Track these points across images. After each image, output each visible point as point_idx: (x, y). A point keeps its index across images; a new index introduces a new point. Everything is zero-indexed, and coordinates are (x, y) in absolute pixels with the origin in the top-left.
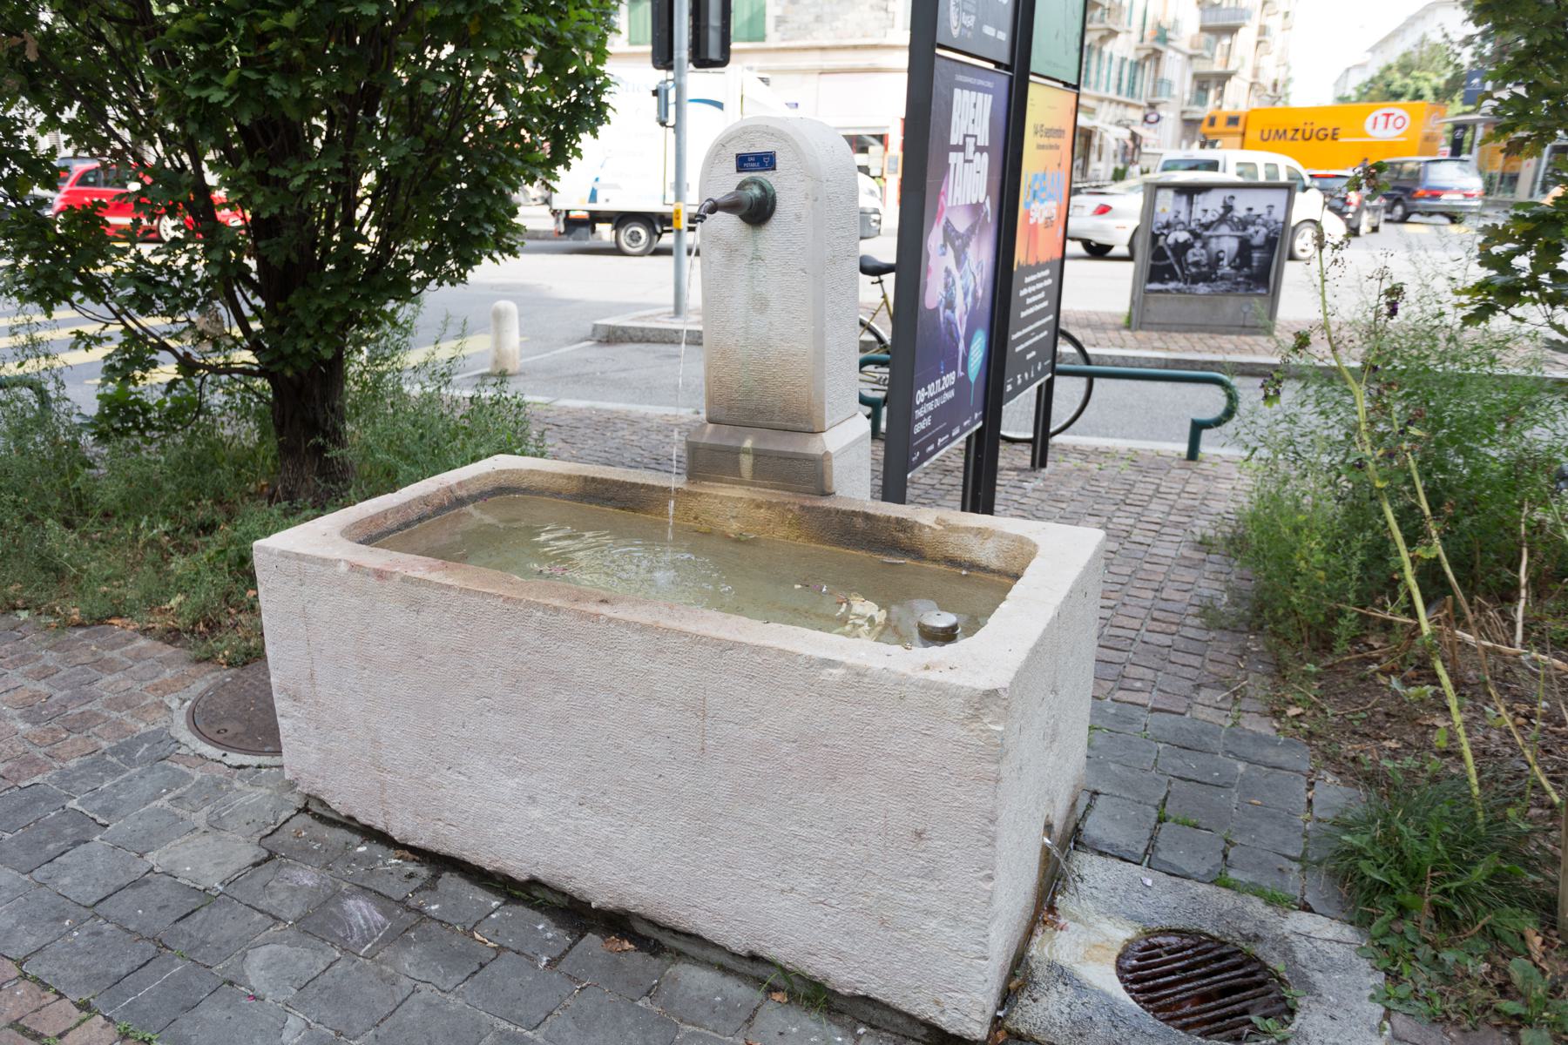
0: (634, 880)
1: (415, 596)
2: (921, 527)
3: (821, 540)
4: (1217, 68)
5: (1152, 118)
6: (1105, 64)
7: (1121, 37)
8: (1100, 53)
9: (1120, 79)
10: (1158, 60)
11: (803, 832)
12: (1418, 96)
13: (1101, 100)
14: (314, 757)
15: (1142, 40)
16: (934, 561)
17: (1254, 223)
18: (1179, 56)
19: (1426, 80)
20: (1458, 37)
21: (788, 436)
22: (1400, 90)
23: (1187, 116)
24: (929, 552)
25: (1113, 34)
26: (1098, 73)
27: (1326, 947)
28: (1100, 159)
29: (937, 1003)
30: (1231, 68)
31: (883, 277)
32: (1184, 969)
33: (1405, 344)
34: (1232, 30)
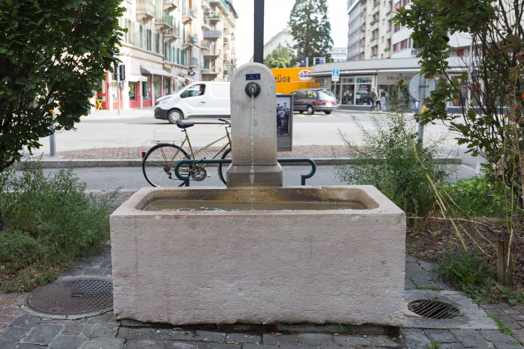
0: (282, 308)
1: (193, 223)
2: (320, 190)
3: (285, 200)
4: (211, 54)
5: (192, 73)
6: (172, 51)
7: (177, 40)
8: (170, 47)
9: (178, 57)
10: (191, 50)
11: (346, 272)
12: (281, 67)
13: (172, 65)
14: (132, 299)
15: (184, 42)
16: (325, 201)
17: (280, 110)
18: (198, 49)
19: (283, 61)
20: (292, 46)
21: (266, 167)
22: (275, 64)
23: (203, 73)
24: (323, 198)
25: (174, 39)
26: (170, 54)
27: (454, 296)
28: (174, 90)
29: (390, 317)
30: (217, 54)
31: (186, 129)
32: (426, 308)
33: (360, 148)
34: (215, 39)
